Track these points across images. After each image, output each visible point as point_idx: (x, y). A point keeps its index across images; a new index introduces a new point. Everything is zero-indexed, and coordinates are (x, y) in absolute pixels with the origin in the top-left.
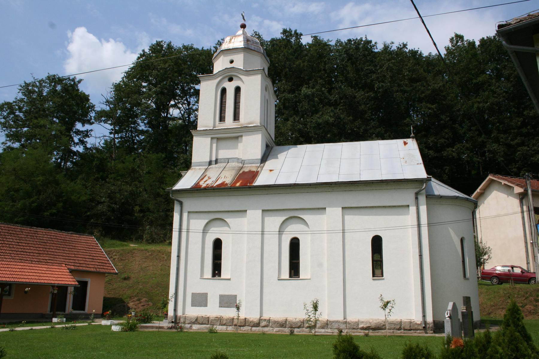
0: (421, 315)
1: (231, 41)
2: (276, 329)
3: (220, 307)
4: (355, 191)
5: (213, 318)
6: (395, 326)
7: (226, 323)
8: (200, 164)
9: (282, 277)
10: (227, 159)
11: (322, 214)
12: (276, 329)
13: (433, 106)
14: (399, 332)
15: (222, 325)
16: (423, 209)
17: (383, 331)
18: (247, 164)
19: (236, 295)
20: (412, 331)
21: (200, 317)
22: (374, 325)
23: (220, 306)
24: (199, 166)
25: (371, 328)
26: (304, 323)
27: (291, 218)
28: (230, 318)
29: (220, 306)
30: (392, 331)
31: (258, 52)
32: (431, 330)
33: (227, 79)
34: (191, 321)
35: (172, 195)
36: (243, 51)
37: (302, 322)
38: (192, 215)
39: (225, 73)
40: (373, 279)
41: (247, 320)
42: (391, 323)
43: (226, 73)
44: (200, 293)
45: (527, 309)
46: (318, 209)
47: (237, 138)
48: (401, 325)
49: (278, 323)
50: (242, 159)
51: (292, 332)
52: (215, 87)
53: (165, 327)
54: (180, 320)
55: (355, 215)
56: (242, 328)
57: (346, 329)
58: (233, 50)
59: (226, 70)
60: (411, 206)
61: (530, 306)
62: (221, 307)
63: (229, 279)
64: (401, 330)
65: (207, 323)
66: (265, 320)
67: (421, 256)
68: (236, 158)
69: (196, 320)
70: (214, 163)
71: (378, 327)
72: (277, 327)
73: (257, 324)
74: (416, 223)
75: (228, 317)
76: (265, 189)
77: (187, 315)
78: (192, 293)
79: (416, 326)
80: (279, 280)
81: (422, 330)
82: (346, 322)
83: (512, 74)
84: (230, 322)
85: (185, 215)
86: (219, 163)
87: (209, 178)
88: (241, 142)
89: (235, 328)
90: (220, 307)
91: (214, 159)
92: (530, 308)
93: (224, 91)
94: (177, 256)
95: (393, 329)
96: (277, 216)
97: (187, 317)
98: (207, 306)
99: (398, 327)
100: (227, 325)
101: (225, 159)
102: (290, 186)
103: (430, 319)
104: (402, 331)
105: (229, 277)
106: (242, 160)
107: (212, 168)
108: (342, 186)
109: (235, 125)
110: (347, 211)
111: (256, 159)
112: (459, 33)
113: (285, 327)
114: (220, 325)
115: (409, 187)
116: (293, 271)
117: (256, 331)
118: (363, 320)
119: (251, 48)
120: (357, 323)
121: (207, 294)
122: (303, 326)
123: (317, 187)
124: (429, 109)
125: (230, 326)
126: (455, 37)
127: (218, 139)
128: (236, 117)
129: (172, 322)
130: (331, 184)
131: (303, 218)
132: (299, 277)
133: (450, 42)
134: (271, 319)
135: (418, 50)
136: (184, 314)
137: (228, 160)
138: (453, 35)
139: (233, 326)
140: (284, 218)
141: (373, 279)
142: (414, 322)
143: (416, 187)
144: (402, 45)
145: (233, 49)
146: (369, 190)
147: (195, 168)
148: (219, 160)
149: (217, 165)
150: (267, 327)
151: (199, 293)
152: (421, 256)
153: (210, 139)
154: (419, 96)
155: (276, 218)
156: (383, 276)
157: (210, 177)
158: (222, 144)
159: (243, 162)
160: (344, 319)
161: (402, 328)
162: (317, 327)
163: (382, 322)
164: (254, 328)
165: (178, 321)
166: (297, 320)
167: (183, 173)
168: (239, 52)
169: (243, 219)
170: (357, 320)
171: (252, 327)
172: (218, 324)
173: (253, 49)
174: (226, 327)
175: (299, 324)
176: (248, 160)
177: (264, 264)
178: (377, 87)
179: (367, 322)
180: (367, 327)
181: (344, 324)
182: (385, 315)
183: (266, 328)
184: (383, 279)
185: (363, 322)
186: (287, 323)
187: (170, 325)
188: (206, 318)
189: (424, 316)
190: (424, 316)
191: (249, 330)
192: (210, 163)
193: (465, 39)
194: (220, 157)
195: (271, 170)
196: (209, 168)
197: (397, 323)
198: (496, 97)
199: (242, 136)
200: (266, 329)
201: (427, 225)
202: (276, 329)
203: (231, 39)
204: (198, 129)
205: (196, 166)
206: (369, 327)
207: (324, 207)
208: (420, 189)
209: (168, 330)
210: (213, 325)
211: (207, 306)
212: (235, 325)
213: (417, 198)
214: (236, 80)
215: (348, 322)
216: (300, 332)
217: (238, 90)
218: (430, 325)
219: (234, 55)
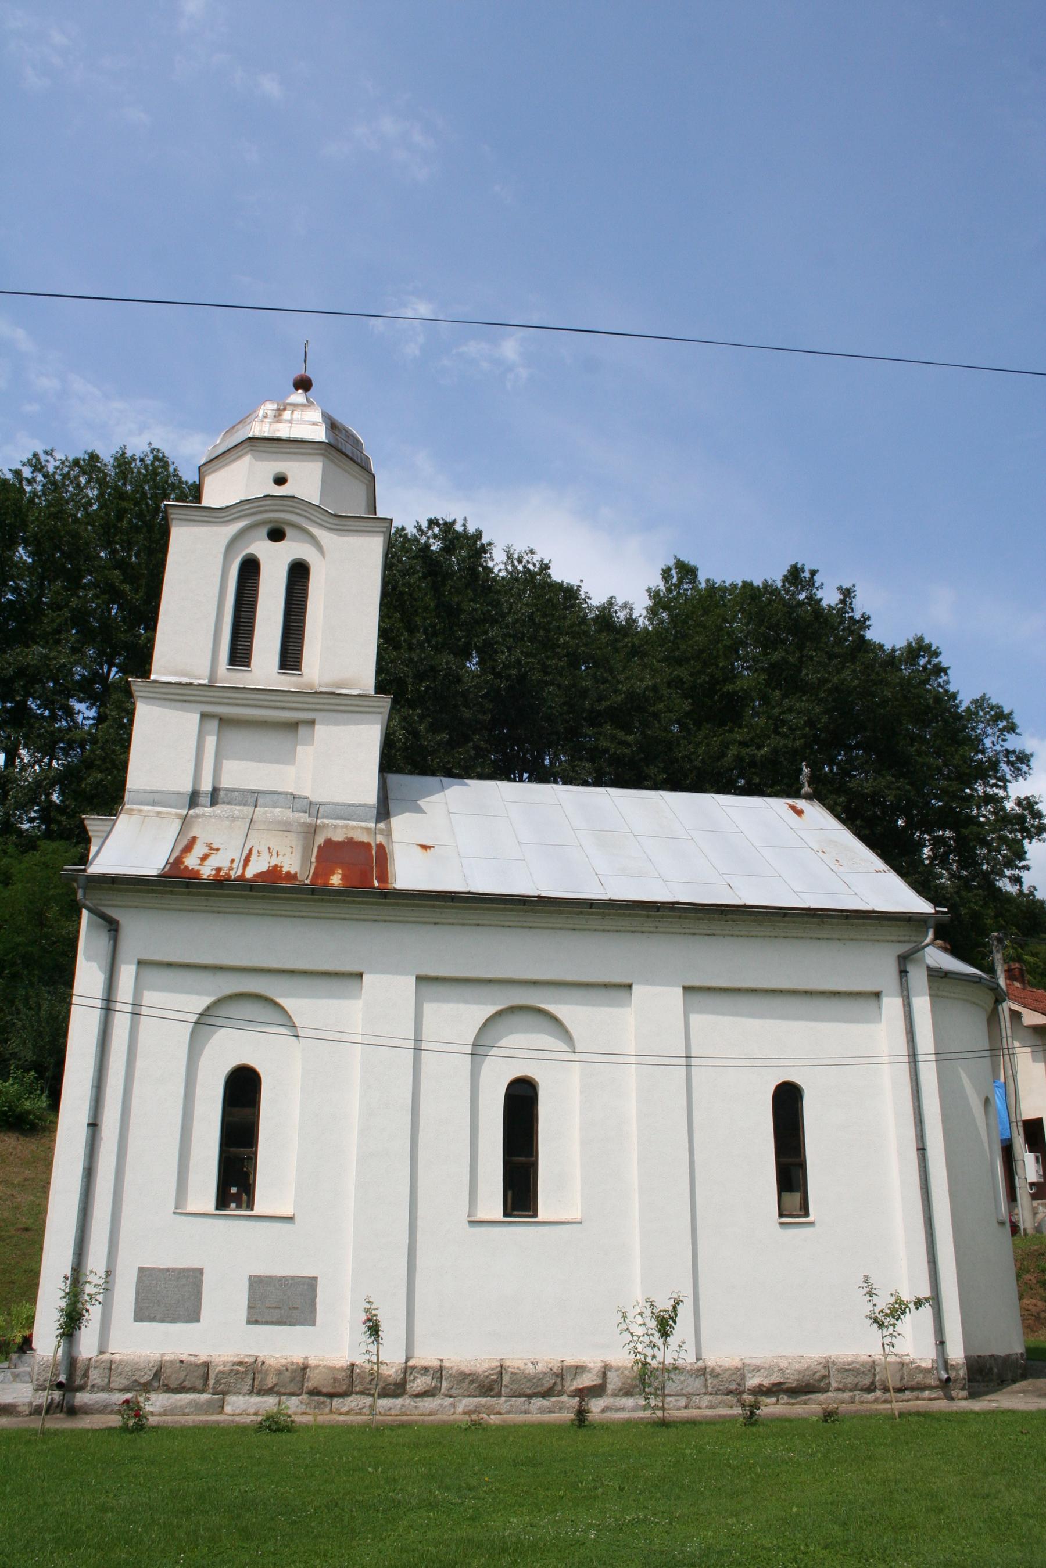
0: (931, 1339)
1: (280, 415)
2: (466, 1401)
3: (249, 1322)
4: (724, 936)
5: (224, 1364)
6: (856, 1380)
7: (276, 1385)
8: (158, 799)
9: (481, 1216)
10: (253, 792)
11: (620, 1005)
12: (466, 1403)
13: (630, 738)
14: (870, 1397)
15: (258, 1394)
16: (922, 1004)
17: (821, 1397)
18: (327, 817)
20: (908, 1394)
21: (171, 1362)
22: (796, 1377)
23: (252, 1321)
24: (154, 804)
25: (785, 1387)
26: (562, 1379)
27: (512, 1010)
28: (292, 1364)
29: (252, 1321)
30: (847, 1395)
31: (362, 467)
32: (963, 1389)
33: (264, 531)
34: (136, 1381)
35: (85, 895)
36: (322, 455)
37: (557, 1375)
38: (152, 975)
39: (261, 512)
40: (781, 1224)
41: (357, 1370)
42: (846, 1370)
43: (266, 511)
44: (174, 1270)
45: (1027, 1310)
46: (606, 986)
47: (293, 726)
48: (875, 1375)
49: (472, 1382)
50: (313, 799)
51: (581, 1414)
52: (223, 549)
53: (20, 1409)
54: (86, 1375)
55: (722, 1014)
56: (336, 1402)
57: (705, 1394)
58: (291, 445)
59: (269, 502)
60: (887, 996)
61: (1033, 1301)
62: (256, 1322)
63: (290, 1219)
64: (874, 1391)
65: (200, 1387)
66: (426, 1370)
67: (922, 1150)
68: (285, 794)
69: (157, 1375)
70: (205, 800)
71: (808, 1385)
72: (469, 1396)
73: (396, 1384)
74: (903, 1049)
75: (283, 1361)
76: (434, 906)
77: (117, 1357)
78: (141, 1270)
79: (919, 1377)
80: (473, 1223)
81: (936, 1387)
82: (702, 1372)
83: (826, 681)
84: (292, 1380)
85: (127, 973)
86: (224, 803)
87: (213, 849)
88: (310, 741)
89: (313, 1404)
90: (249, 1322)
91: (206, 786)
92: (1035, 1305)
93: (250, 569)
94: (89, 1125)
95: (851, 1390)
96: (466, 1002)
97: (120, 1362)
98: (198, 1320)
99: (866, 1381)
100: (279, 1394)
101: (244, 791)
102: (785, 915)
103: (956, 1353)
104: (878, 1393)
105: (288, 1212)
106: (311, 803)
107: (203, 815)
108: (686, 918)
109: (286, 682)
110: (698, 999)
111: (360, 805)
112: (685, 558)
113: (499, 1395)
114: (251, 1392)
115: (880, 938)
116: (510, 1193)
117: (393, 1412)
118: (757, 1362)
119: (344, 450)
120: (740, 1372)
121: (200, 1271)
122: (559, 1388)
123: (609, 915)
124: (621, 743)
125: (293, 1394)
126: (676, 568)
127: (225, 722)
129: (60, 1386)
130: (658, 909)
131: (560, 1016)
132: (535, 1215)
133: (663, 578)
134: (446, 1364)
135: (578, 583)
136: (101, 1353)
137: (254, 797)
138: (671, 563)
139: (305, 1397)
140: (492, 1009)
141: (781, 1224)
142: (911, 1363)
143: (902, 938)
144: (538, 565)
145: (289, 441)
146: (765, 936)
147: (140, 811)
148: (222, 794)
149: (218, 810)
150: (433, 1395)
151: (168, 1270)
152: (922, 1150)
153: (198, 717)
154: (592, 705)
155: (462, 1006)
156: (807, 1214)
157: (215, 846)
158: (238, 739)
159: (311, 807)
160: (698, 1359)
161: (877, 1384)
162: (609, 1392)
163: (820, 1367)
164: (383, 1403)
165: (78, 1382)
166: (541, 1367)
167: (94, 824)
168: (310, 454)
169: (353, 1002)
170: (736, 1363)
172: (246, 1388)
173: (350, 454)
174: (277, 1400)
175: (548, 1383)
176: (333, 804)
177: (420, 1166)
178: (503, 663)
179: (770, 1370)
180: (774, 1385)
181: (697, 1376)
182: (883, 1345)
183: (430, 1399)
184: (812, 1224)
185: (758, 1369)
186: (506, 1379)
187: (42, 1398)
188: (197, 1366)
189: (941, 1343)
190: (941, 1343)
191: (366, 1411)
192: (194, 799)
193: (702, 577)
194: (226, 783)
195: (425, 847)
196: (192, 816)
197: (862, 1369)
198: (785, 736)
199: (312, 723)
200: (429, 1404)
201: (933, 1057)
202: (466, 1403)
203: (278, 410)
204: (153, 677)
205: (141, 804)
206: (780, 1384)
207: (626, 981)
208: (914, 945)
209: (36, 1423)
210: (224, 1393)
211: (198, 1320)
212: (314, 1392)
213: (903, 973)
214: (294, 540)
215: (713, 1370)
216: (550, 1412)
217: (299, 573)
218: (957, 1370)
219: (291, 460)
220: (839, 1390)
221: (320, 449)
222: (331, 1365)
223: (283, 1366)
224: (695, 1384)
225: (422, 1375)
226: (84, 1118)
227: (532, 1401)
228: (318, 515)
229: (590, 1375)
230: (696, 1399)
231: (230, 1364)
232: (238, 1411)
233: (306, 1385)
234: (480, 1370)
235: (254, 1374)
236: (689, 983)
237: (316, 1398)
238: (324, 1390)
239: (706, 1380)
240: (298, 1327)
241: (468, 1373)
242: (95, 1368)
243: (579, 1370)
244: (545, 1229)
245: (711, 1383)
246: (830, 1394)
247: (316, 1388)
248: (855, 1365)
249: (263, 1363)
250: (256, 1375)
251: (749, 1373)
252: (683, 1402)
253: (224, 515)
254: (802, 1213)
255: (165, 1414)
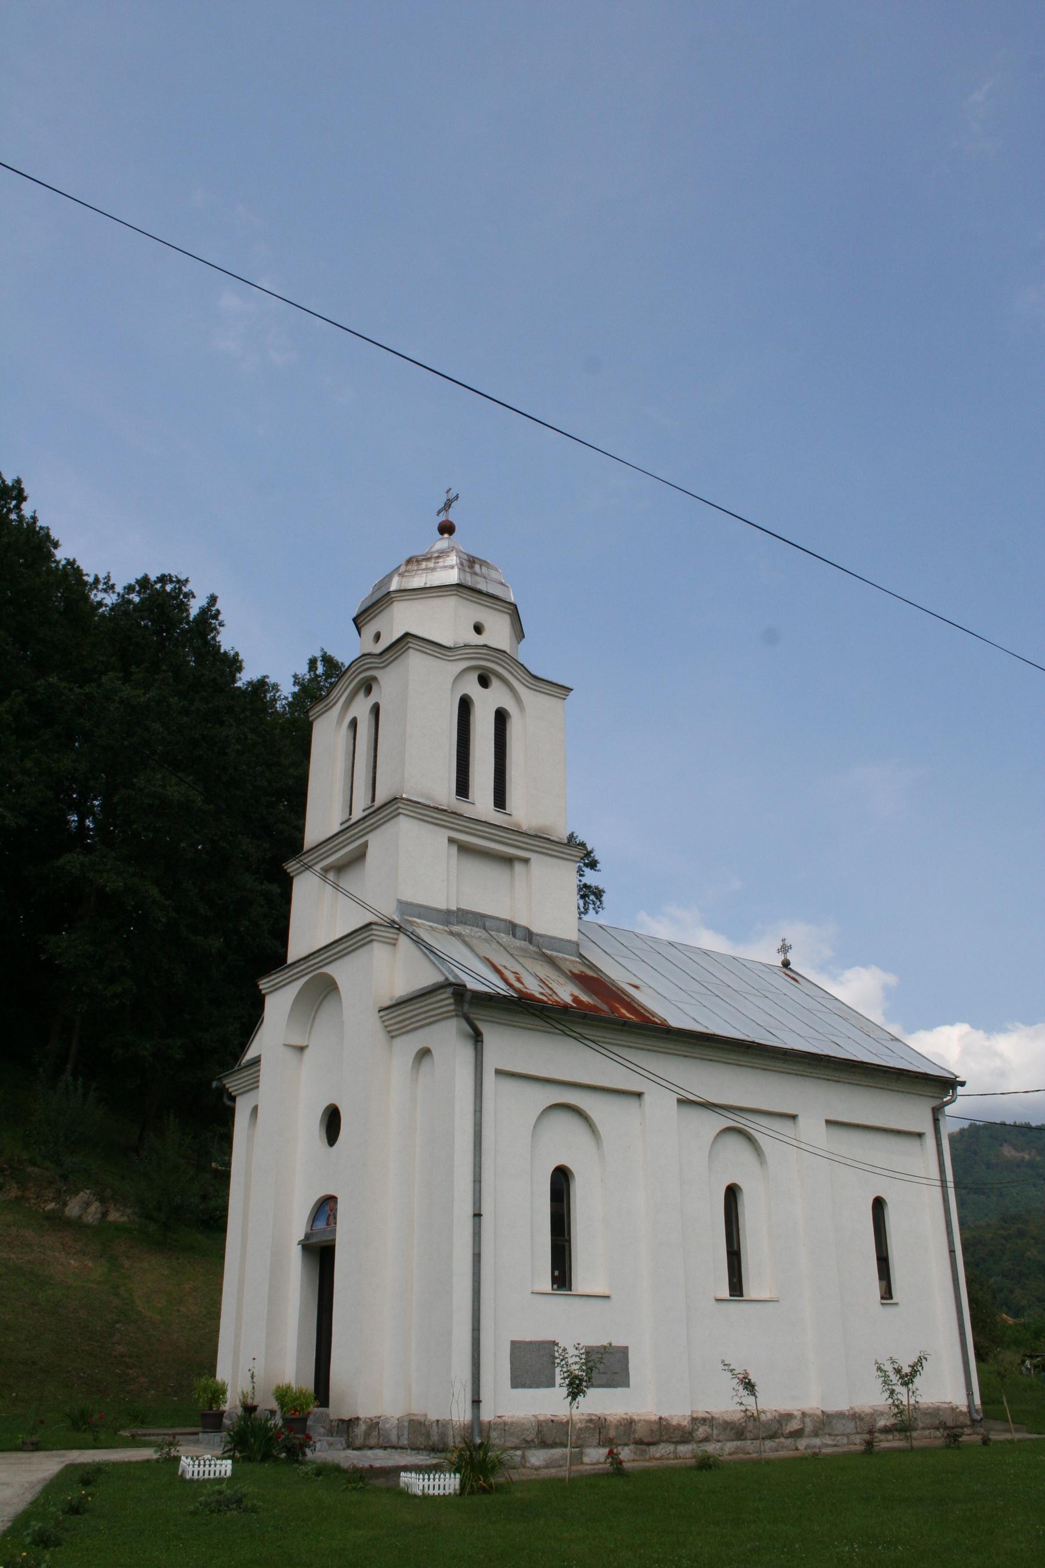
19: (627, 1348)
30: (927, 1432)
40: (882, 1304)
47: (509, 861)
49: (732, 1429)
72: (733, 1440)
93: (465, 706)
102: (886, 1072)
105: (606, 1293)
113: (745, 1439)
127: (464, 849)
128: (500, 800)
138: (318, 654)
141: (882, 1304)
151: (531, 1343)
156: (891, 1297)
162: (806, 1433)
171: (677, 1443)
212: (639, 1442)
217: (501, 718)
220: (923, 1428)
221: (509, 609)
222: (648, 1419)
223: (618, 1421)
224: (850, 1426)
225: (702, 1424)
226: (469, 1211)
227: (765, 1443)
228: (522, 674)
229: (796, 1421)
230: (852, 1437)
231: (585, 1421)
232: (594, 1461)
233: (632, 1437)
234: (736, 1419)
235: (599, 1429)
236: (832, 1118)
237: (640, 1447)
238: (646, 1440)
239: (856, 1423)
240: (619, 1388)
241: (729, 1421)
242: (494, 1430)
243: (789, 1416)
244: (577, 1300)
245: (859, 1425)
246: (918, 1432)
247: (640, 1439)
248: (929, 1410)
249: (606, 1419)
250: (602, 1430)
251: (878, 1417)
252: (845, 1441)
253: (451, 654)
254: (888, 1296)
255: (547, 1467)
